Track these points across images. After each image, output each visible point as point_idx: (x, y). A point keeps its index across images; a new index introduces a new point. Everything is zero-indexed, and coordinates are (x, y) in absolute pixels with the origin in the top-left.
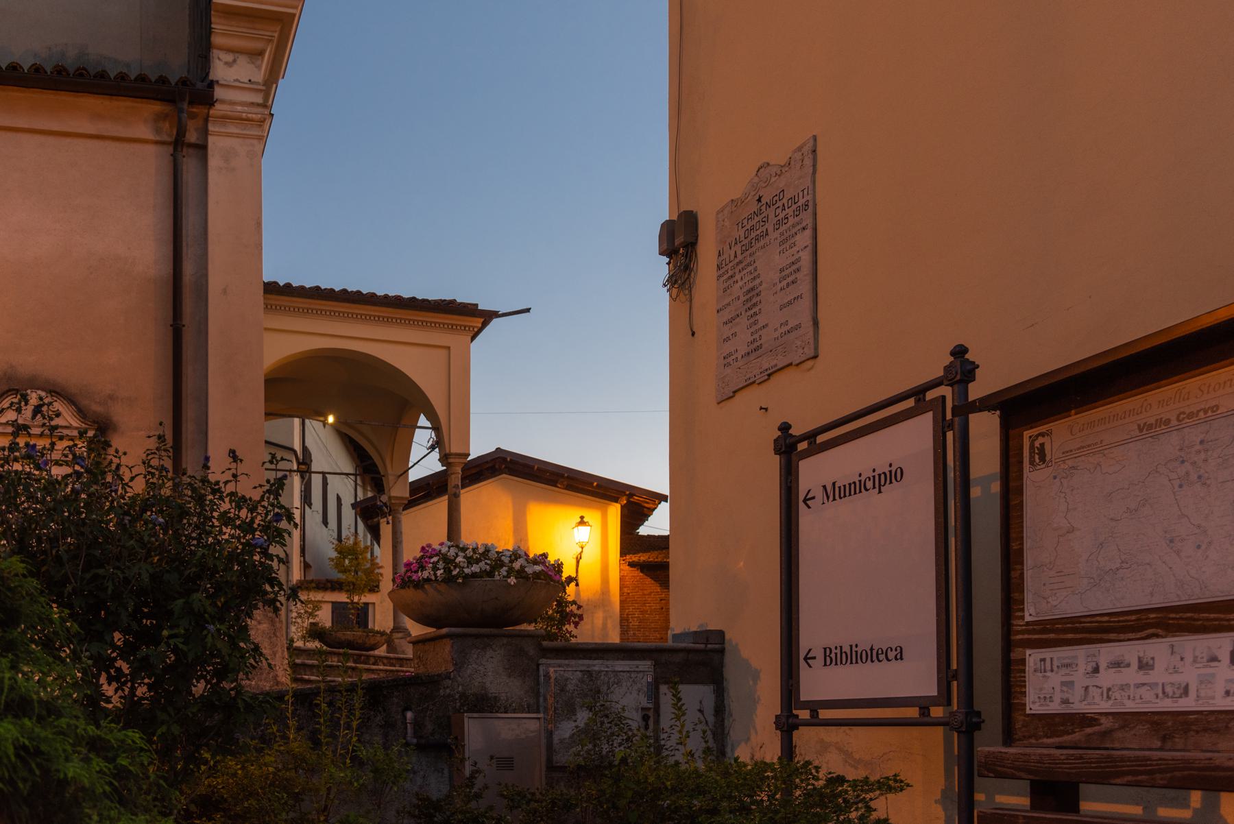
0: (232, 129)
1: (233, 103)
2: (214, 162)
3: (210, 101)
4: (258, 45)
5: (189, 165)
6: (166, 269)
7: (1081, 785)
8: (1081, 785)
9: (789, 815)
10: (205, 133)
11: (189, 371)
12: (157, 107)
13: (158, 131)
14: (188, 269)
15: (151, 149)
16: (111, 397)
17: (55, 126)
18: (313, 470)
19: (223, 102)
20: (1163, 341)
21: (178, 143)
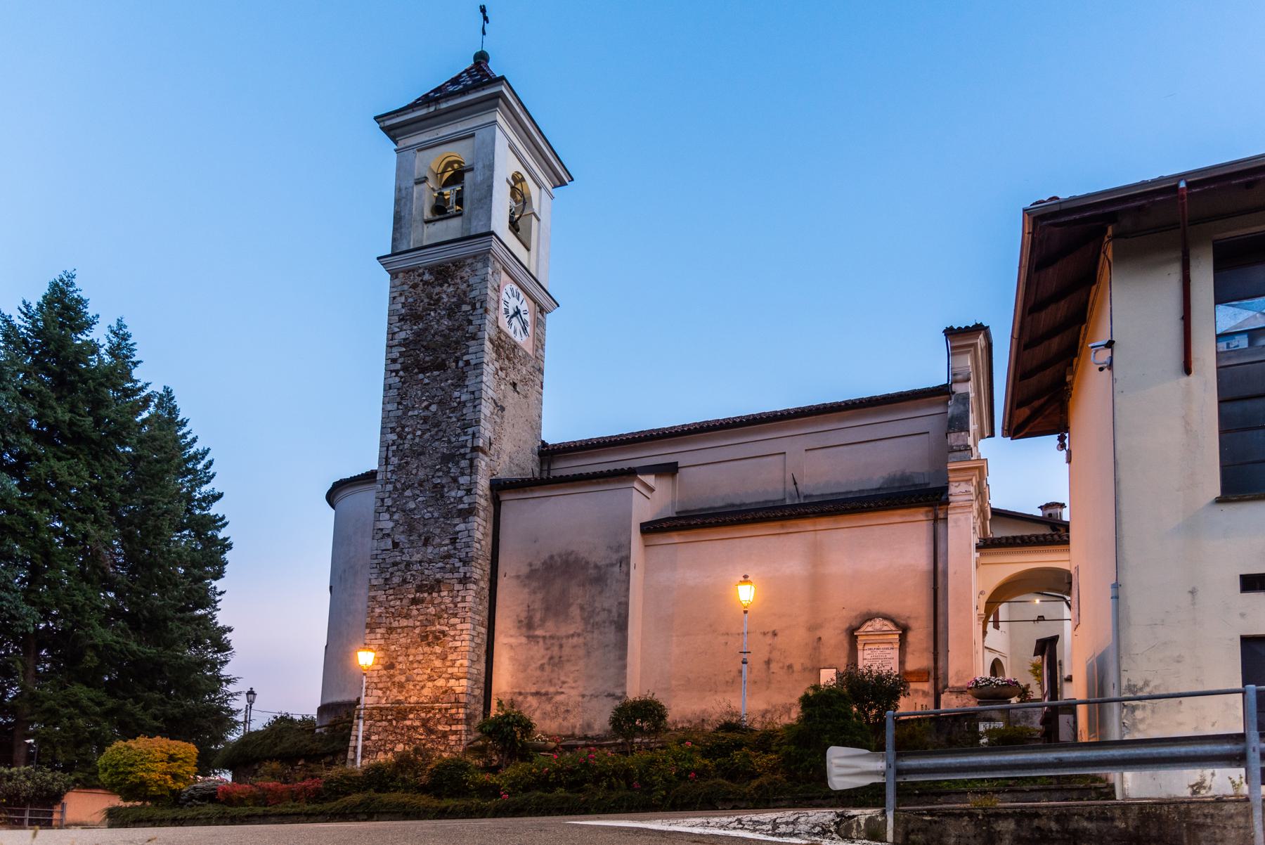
0: (959, 511)
1: (957, 502)
2: (950, 525)
3: (947, 502)
4: (970, 478)
5: (941, 526)
6: (931, 567)
7: (1078, 706)
8: (1078, 706)
9: (425, 582)
10: (947, 514)
11: (940, 604)
12: (927, 509)
13: (927, 516)
14: (940, 566)
15: (925, 522)
16: (908, 617)
17: (883, 522)
18: (896, 669)
19: (953, 502)
20: (321, 825)
21: (936, 520)
